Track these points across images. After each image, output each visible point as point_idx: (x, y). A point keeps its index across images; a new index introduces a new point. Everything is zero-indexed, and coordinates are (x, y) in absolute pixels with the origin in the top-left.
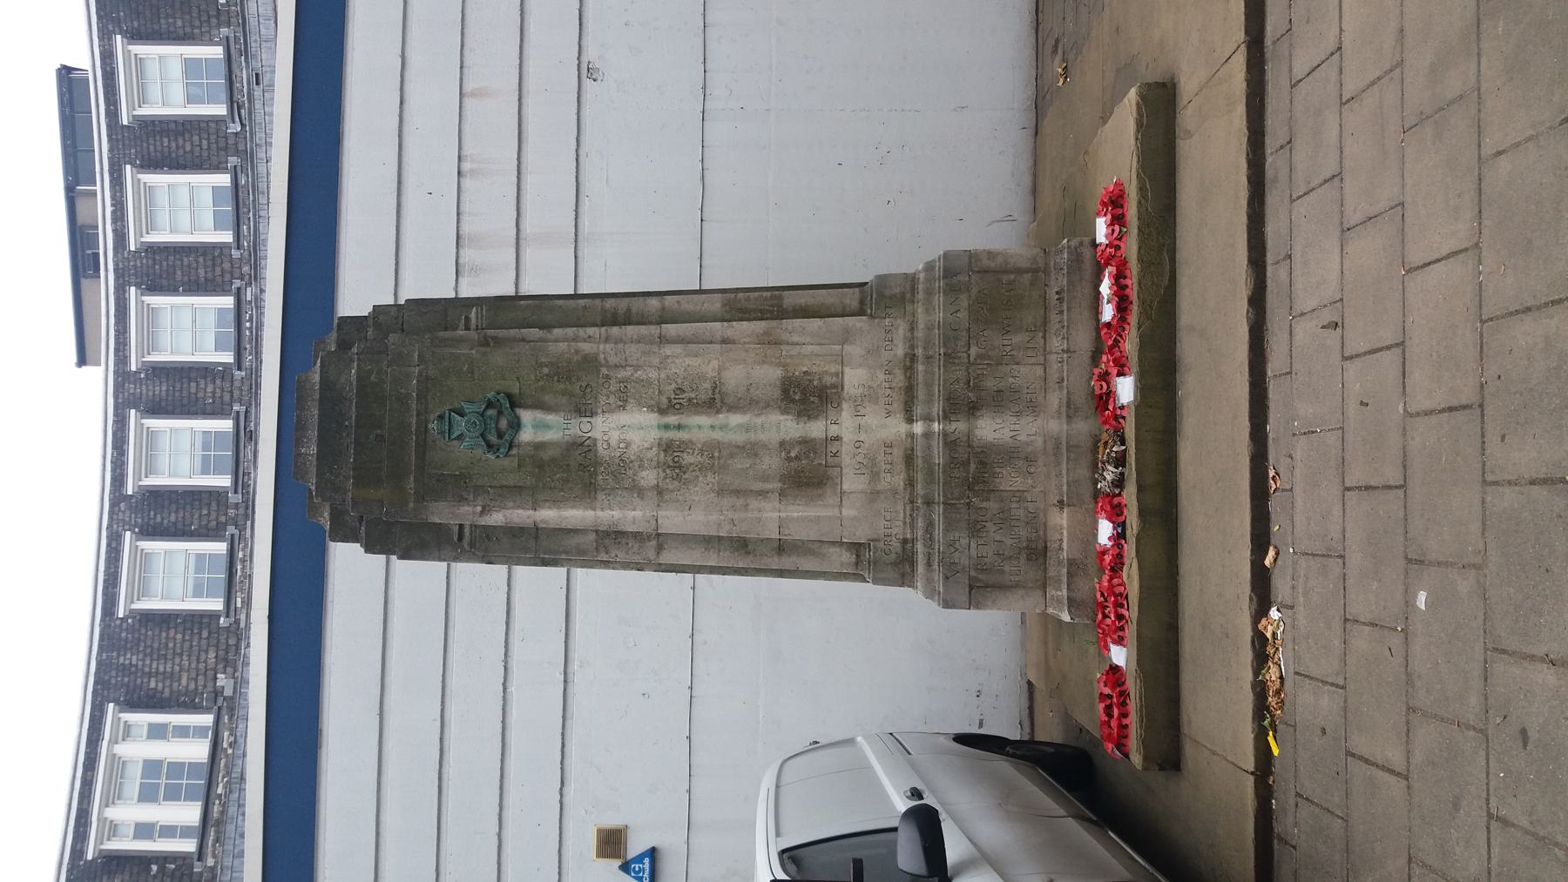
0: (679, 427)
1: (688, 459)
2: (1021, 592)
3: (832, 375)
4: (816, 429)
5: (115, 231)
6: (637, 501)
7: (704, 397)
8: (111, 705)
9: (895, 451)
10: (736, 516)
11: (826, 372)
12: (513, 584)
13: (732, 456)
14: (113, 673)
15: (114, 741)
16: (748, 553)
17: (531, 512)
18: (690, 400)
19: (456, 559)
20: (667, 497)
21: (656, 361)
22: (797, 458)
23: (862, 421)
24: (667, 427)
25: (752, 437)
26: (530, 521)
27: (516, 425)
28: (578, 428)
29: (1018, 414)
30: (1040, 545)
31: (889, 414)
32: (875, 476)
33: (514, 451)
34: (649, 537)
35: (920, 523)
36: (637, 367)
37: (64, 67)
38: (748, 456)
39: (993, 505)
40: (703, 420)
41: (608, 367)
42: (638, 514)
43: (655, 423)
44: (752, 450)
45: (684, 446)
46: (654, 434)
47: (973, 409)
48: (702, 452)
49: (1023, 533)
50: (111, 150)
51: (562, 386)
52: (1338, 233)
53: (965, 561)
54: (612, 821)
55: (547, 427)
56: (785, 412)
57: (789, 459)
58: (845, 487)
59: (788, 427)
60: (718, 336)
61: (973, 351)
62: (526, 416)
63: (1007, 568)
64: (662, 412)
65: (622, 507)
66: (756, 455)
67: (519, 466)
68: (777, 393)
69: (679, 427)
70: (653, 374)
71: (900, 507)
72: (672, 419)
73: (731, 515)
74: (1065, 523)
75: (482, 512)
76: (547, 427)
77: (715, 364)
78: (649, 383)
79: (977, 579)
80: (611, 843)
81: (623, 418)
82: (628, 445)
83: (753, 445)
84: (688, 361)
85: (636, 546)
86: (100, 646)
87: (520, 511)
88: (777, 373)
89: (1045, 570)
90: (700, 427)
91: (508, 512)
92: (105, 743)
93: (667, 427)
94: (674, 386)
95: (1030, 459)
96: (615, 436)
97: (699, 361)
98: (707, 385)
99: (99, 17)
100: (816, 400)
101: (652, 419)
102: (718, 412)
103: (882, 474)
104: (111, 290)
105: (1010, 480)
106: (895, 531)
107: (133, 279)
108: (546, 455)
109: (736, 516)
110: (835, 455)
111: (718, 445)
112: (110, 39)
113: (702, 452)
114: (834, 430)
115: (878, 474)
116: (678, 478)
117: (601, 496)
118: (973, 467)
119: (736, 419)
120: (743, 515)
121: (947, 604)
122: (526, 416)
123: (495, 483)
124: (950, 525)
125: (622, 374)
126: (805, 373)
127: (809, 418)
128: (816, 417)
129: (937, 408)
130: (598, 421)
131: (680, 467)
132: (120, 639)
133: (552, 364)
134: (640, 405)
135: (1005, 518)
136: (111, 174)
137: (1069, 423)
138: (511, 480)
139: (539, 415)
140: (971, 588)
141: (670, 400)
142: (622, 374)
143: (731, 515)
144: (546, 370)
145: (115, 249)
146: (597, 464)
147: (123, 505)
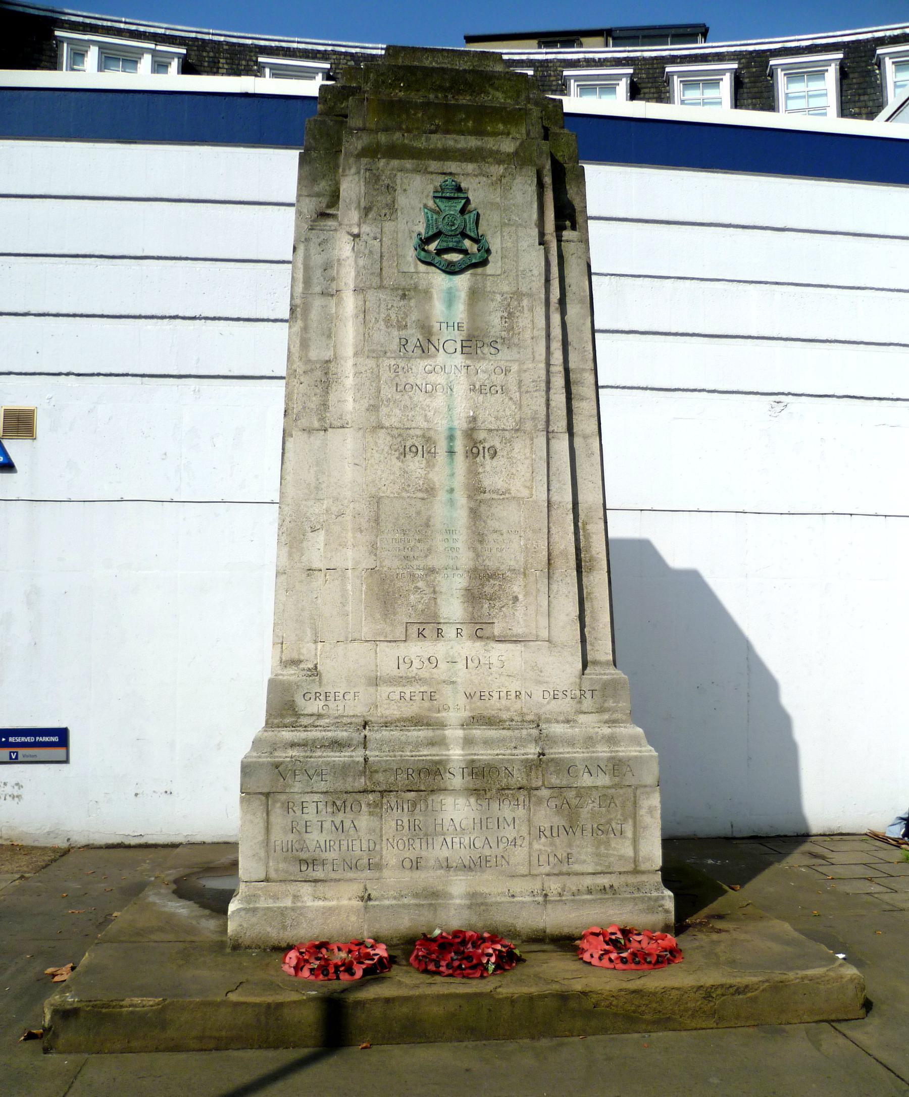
0: (451, 452)
5: (579, 60)
6: (365, 403)
7: (487, 482)
8: (184, 51)
10: (348, 517)
14: (211, 54)
15: (154, 53)
17: (352, 286)
19: (299, 213)
24: (451, 438)
26: (342, 286)
27: (451, 270)
34: (322, 419)
35: (342, 734)
37: (707, 30)
41: (519, 372)
42: (350, 405)
43: (456, 424)
46: (441, 425)
50: (644, 59)
54: (41, 424)
60: (555, 498)
64: (470, 434)
65: (358, 388)
69: (451, 452)
72: (459, 445)
73: (349, 511)
74: (345, 902)
80: (21, 423)
85: (313, 406)
86: (234, 44)
87: (353, 274)
90: (453, 475)
91: (351, 261)
92: (152, 46)
93: (451, 438)
94: (498, 446)
99: (751, 52)
101: (460, 424)
104: (532, 57)
106: (332, 705)
107: (539, 74)
109: (348, 517)
110: (420, 634)
112: (734, 60)
114: (450, 631)
117: (371, 363)
120: (350, 526)
121: (247, 769)
122: (462, 281)
124: (344, 770)
129: (484, 754)
132: (240, 59)
136: (625, 58)
137: (412, 812)
139: (463, 295)
143: (349, 511)
145: (564, 60)
147: (352, 63)
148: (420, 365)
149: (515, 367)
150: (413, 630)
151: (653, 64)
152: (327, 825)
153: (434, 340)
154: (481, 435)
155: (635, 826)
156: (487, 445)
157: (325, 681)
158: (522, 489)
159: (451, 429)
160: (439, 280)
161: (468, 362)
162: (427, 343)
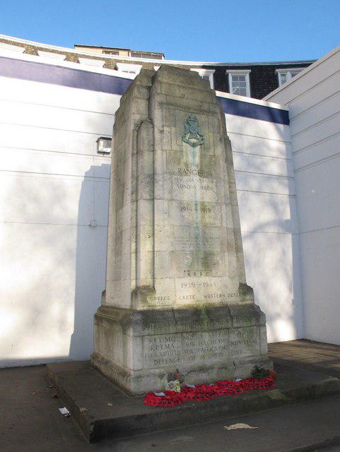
28: (195, 169)
55: (194, 157)
69: (196, 210)
76: (194, 157)
81: (198, 188)
93: (196, 205)
130: (197, 178)
148: (185, 178)
150: (186, 273)
152: (164, 346)
162: (185, 172)
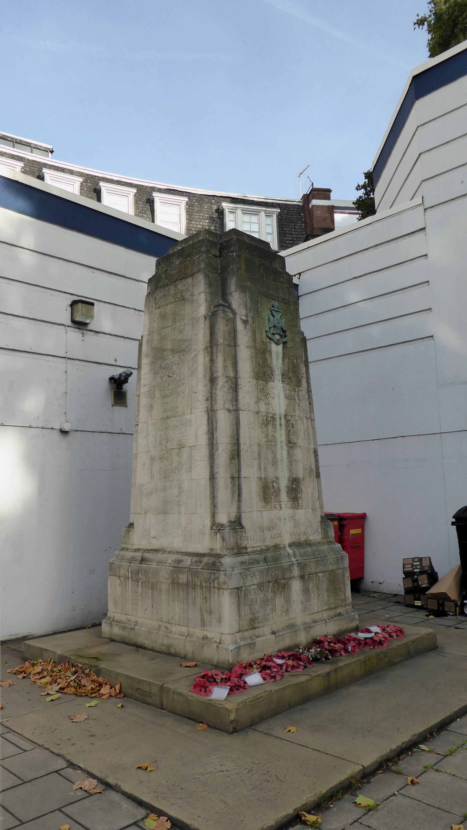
0: (281, 425)
1: (270, 428)
2: (237, 618)
3: (302, 503)
4: (284, 496)
9: (279, 539)
11: (302, 501)
12: (32, 321)
13: (272, 452)
16: (231, 460)
18: (290, 431)
20: (256, 415)
21: (301, 415)
22: (273, 486)
23: (287, 521)
24: (280, 418)
25: (279, 463)
29: (302, 602)
30: (256, 625)
31: (291, 534)
32: (269, 529)
33: (268, 340)
36: (298, 405)
38: (273, 460)
39: (270, 595)
40: (284, 438)
44: (275, 463)
45: (274, 426)
46: (277, 412)
47: (302, 577)
48: (273, 436)
49: (261, 615)
51: (291, 368)
52: (58, 807)
53: (248, 583)
56: (289, 480)
57: (273, 482)
58: (264, 512)
59: (284, 483)
61: (321, 575)
62: (280, 347)
63: (246, 607)
64: (285, 416)
66: (273, 465)
67: (263, 342)
68: (295, 476)
70: (297, 413)
71: (259, 544)
72: (283, 421)
75: (242, 319)
76: (277, 359)
77: (302, 445)
78: (294, 411)
79: (241, 591)
81: (282, 396)
82: (273, 398)
83: (276, 462)
84: (302, 430)
88: (301, 476)
89: (247, 630)
93: (280, 418)
94: (294, 423)
95: (287, 611)
96: (276, 391)
97: (303, 437)
98: (295, 440)
100: (293, 496)
101: (283, 413)
102: (287, 445)
103: (270, 533)
105: (279, 601)
106: (250, 542)
108: (267, 355)
111: (275, 445)
113: (273, 436)
115: (270, 531)
116: (263, 423)
118: (283, 581)
119: (285, 453)
123: (256, 329)
125: (296, 397)
126: (302, 490)
127: (287, 492)
128: (288, 497)
131: (267, 424)
133: (297, 364)
134: (287, 405)
135: (265, 602)
138: (258, 336)
140: (237, 589)
141: (289, 421)
142: (296, 397)
144: (295, 361)
146: (266, 381)
149: (297, 389)
151: (33, 164)
153: (273, 373)
154: (289, 418)
155: (344, 586)
156: (291, 422)
157: (246, 531)
158: (301, 442)
159: (280, 414)
160: (273, 346)
161: (284, 385)
